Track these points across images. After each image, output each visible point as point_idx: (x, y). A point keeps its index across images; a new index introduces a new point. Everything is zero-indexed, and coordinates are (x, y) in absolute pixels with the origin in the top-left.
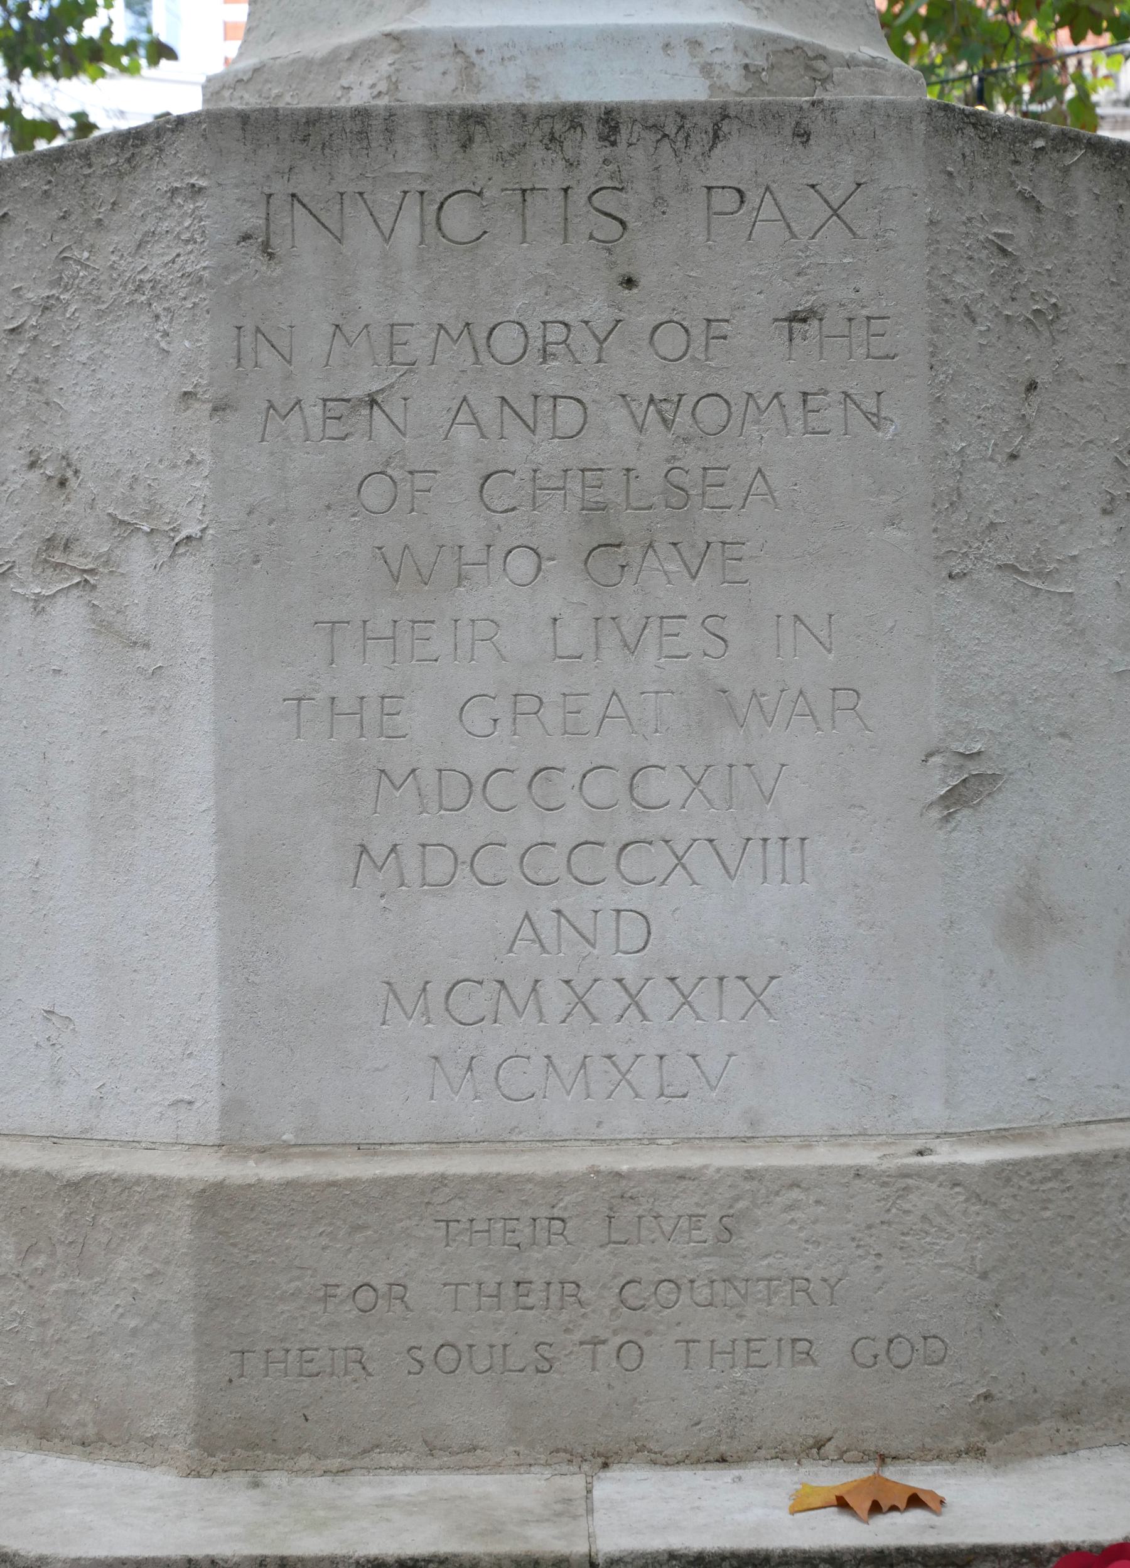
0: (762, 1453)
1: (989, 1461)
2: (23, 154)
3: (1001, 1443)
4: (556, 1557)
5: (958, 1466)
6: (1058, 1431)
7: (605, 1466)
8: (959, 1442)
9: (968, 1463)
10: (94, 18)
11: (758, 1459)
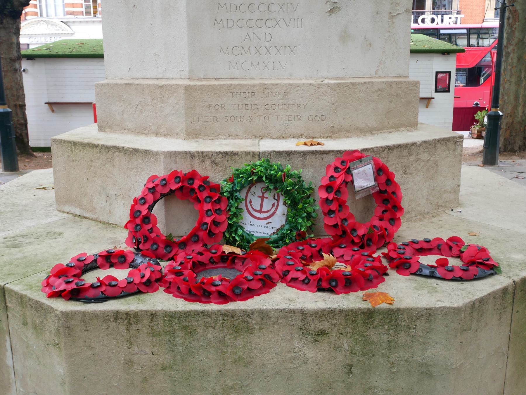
8: (327, 135)
9: (329, 139)
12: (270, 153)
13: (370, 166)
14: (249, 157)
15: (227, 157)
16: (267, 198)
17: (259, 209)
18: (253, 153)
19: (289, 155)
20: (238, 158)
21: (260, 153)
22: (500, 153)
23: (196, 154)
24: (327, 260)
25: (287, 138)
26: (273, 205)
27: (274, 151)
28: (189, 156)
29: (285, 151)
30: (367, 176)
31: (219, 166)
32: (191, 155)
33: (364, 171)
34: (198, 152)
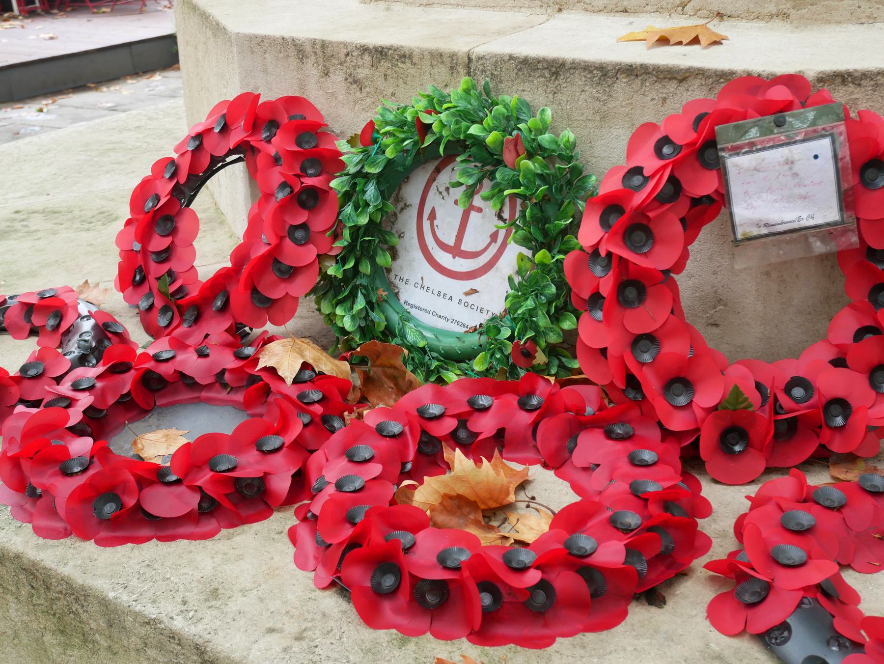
0: (648, 8)
1: (791, 22)
2: (62, 443)
3: (804, 11)
4: (450, 53)
5: (769, 25)
6: (859, 7)
7: (560, 10)
8: (772, 8)
9: (777, 23)
10: (171, 74)
11: (646, 12)
12: (500, 61)
13: (824, 146)
14: (442, 72)
15: (385, 65)
16: (480, 210)
17: (451, 242)
18: (453, 56)
19: (556, 74)
20: (412, 71)
21: (470, 60)
22: (187, 294)
23: (308, 49)
24: (460, 479)
25: (635, 12)
26: (494, 237)
27: (511, 57)
28: (292, 52)
29: (545, 60)
30: (799, 185)
31: (365, 90)
32: (299, 51)
33: (790, 162)
34: (314, 42)
